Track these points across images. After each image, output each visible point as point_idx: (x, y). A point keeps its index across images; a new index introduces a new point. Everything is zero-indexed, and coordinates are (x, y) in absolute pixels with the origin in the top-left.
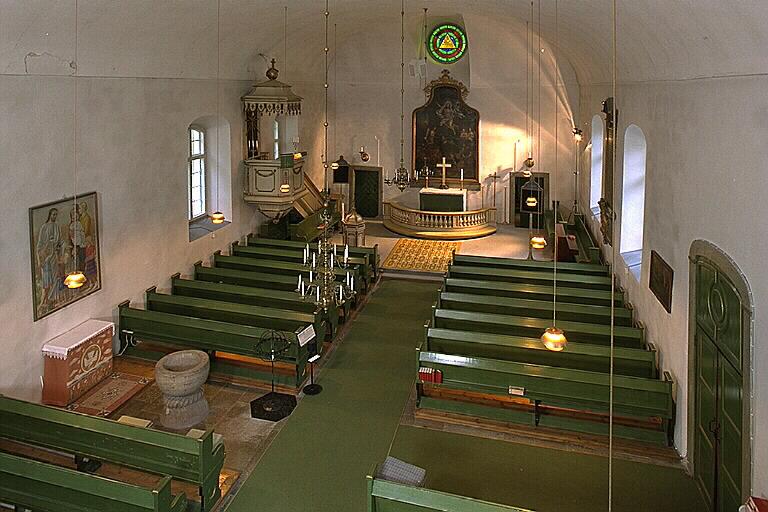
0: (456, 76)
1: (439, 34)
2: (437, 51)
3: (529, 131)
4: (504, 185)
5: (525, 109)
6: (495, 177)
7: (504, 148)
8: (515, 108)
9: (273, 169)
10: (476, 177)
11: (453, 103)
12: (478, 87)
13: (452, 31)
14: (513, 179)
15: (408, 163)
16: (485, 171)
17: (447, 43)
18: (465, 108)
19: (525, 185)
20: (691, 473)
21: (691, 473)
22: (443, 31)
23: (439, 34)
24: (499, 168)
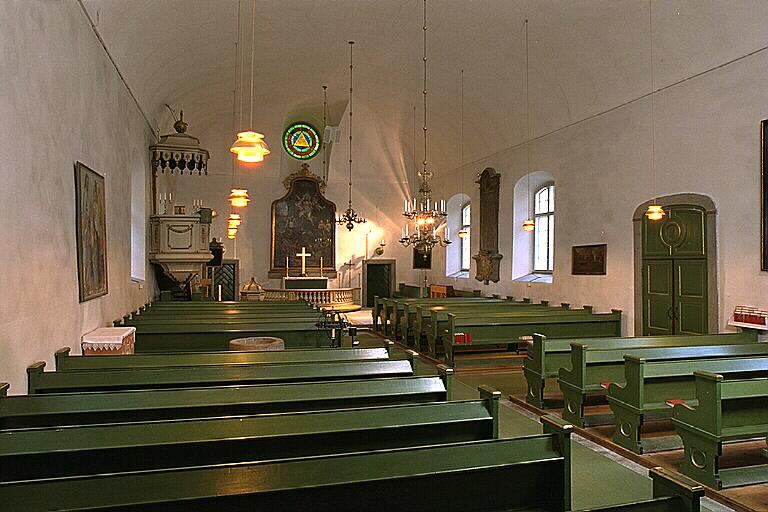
0: (315, 170)
1: (293, 133)
2: (292, 149)
3: (378, 223)
4: (357, 274)
5: (382, 202)
6: (350, 265)
7: (357, 242)
8: (367, 202)
9: (190, 224)
10: (332, 263)
11: (313, 196)
12: (336, 184)
13: (306, 130)
14: (366, 266)
15: (265, 267)
16: (341, 259)
17: (302, 142)
18: (322, 201)
19: (377, 274)
20: (232, 150)
21: (232, 150)
22: (298, 129)
23: (293, 133)
24: (353, 256)
